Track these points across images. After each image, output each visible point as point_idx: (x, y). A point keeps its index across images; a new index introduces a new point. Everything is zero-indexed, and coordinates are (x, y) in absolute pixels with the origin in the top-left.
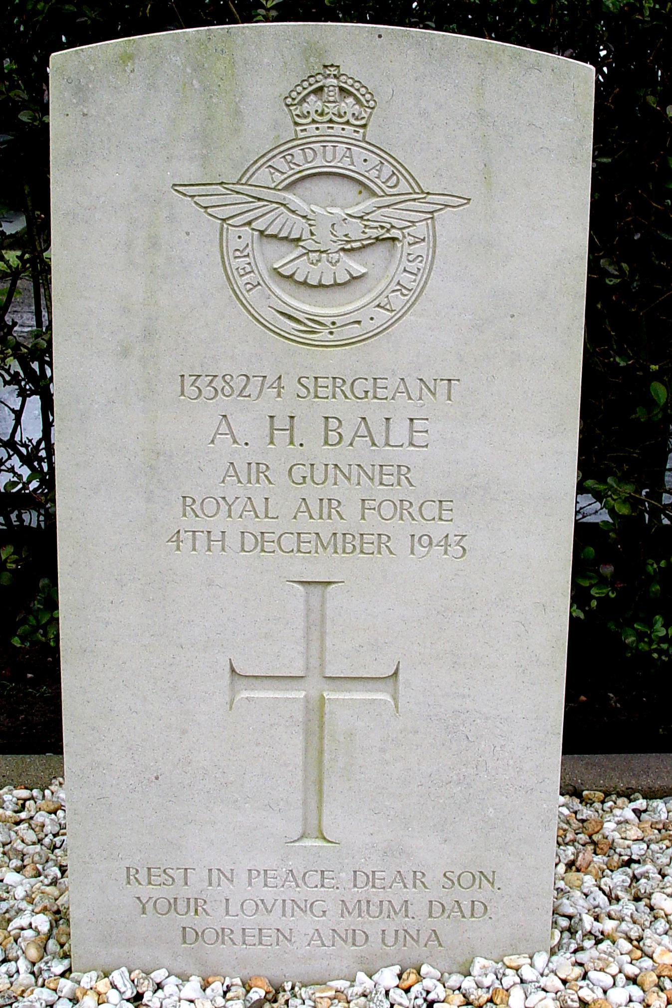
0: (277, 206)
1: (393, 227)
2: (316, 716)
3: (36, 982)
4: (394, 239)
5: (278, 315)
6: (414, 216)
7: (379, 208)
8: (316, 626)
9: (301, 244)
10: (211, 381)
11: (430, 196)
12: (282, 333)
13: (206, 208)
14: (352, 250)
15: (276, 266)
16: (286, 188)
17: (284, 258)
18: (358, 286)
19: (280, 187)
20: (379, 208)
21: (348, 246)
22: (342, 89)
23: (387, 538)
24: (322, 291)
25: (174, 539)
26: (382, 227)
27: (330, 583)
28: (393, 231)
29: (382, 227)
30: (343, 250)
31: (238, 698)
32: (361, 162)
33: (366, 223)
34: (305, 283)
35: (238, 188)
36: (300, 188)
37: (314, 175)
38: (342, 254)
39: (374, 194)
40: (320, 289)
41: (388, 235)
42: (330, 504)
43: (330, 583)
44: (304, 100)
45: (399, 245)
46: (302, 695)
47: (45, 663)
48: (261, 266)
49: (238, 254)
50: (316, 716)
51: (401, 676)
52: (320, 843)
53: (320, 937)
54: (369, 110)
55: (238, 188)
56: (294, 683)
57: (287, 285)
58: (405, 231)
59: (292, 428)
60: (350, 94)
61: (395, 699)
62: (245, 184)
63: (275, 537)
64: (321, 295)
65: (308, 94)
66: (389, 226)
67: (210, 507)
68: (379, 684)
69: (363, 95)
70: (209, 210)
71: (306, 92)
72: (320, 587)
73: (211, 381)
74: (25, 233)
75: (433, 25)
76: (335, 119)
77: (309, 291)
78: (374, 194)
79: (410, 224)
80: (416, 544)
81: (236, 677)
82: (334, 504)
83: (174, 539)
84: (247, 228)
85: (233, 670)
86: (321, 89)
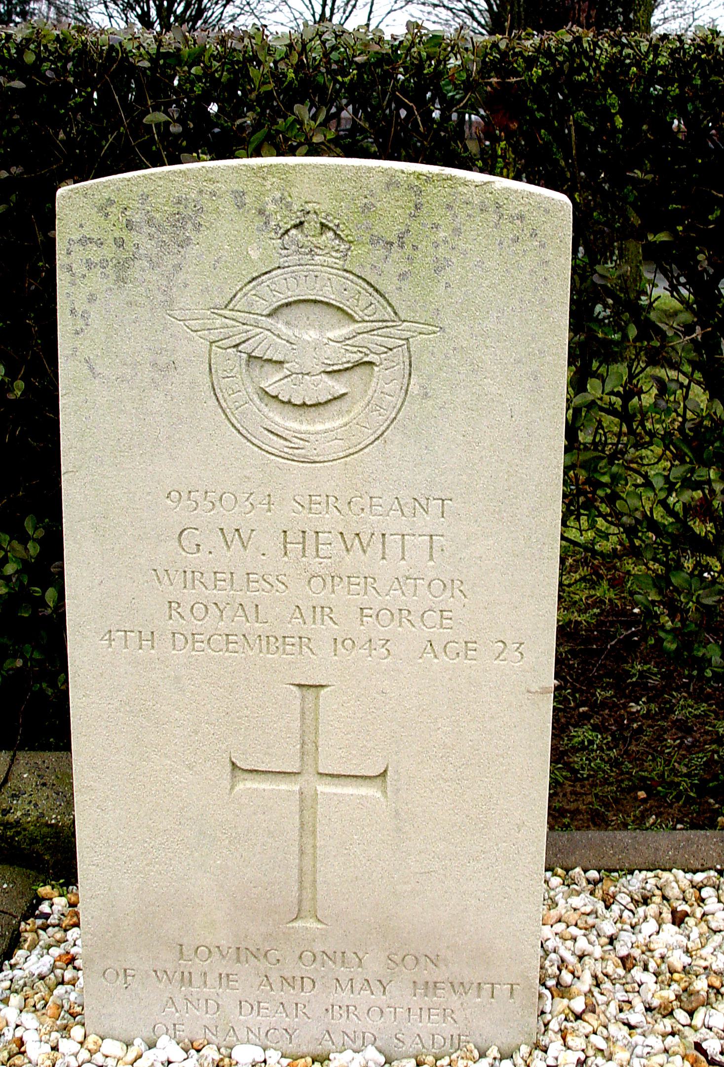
0: (262, 330)
1: (371, 352)
2: (306, 803)
3: (605, 945)
4: (370, 363)
5: (266, 432)
6: (391, 343)
7: (359, 334)
9: (286, 365)
10: (518, 648)
11: (405, 323)
16: (269, 315)
17: (272, 380)
18: (335, 407)
19: (264, 313)
20: (359, 334)
22: (322, 224)
23: (274, 640)
25: (106, 638)
28: (372, 355)
31: (237, 789)
33: (348, 348)
35: (226, 313)
41: (366, 359)
42: (322, 611)
43: (322, 686)
45: (376, 369)
46: (296, 788)
50: (306, 803)
53: (235, 1033)
55: (226, 313)
56: (288, 778)
57: (275, 404)
59: (304, 542)
60: (330, 229)
61: (385, 792)
62: (233, 310)
66: (368, 352)
67: (199, 610)
73: (518, 648)
75: (374, 149)
77: (298, 412)
79: (386, 350)
80: (339, 646)
81: (239, 773)
82: (327, 610)
83: (106, 638)
84: (235, 350)
86: (301, 223)
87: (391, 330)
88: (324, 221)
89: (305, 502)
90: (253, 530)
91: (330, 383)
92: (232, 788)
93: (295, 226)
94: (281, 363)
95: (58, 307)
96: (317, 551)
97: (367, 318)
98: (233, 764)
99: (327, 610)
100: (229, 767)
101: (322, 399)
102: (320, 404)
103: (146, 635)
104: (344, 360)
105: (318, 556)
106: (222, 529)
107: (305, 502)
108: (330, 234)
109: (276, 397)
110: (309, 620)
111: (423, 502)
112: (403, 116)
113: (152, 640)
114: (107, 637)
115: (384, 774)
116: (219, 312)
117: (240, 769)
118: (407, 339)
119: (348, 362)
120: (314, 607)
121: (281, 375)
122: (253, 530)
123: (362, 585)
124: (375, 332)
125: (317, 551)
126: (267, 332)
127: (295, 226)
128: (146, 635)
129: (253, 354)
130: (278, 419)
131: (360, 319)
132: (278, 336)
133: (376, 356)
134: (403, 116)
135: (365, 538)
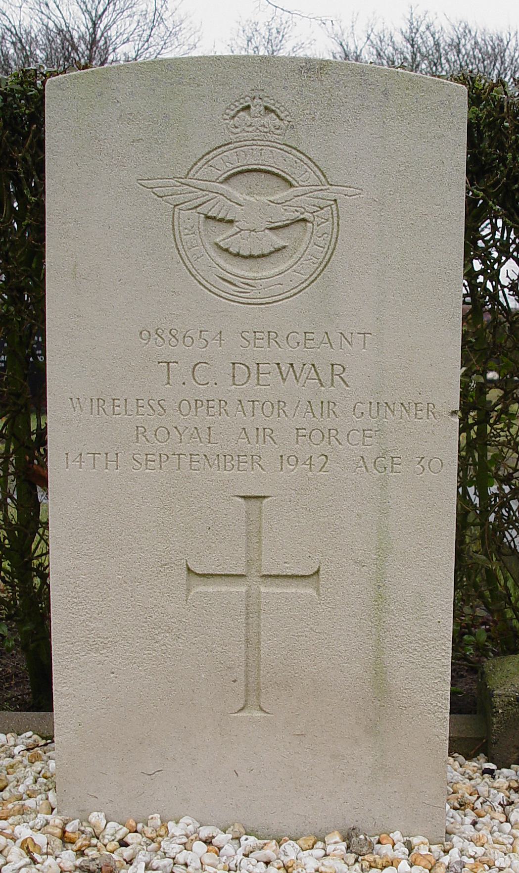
2: (252, 609)
4: (304, 220)
5: (221, 281)
6: (322, 203)
8: (254, 534)
12: (223, 294)
15: (217, 240)
16: (221, 183)
17: (223, 235)
21: (273, 225)
22: (266, 108)
24: (238, 259)
26: (297, 211)
27: (264, 497)
29: (297, 211)
34: (238, 255)
36: (234, 181)
37: (273, 174)
38: (267, 231)
39: (291, 185)
41: (302, 217)
43: (264, 497)
44: (233, 117)
45: (310, 225)
46: (243, 589)
47: (32, 613)
50: (252, 609)
52: (261, 714)
57: (226, 254)
60: (273, 111)
65: (238, 112)
69: (274, 105)
71: (238, 109)
74: (516, 314)
76: (247, 129)
78: (291, 185)
86: (248, 107)
87: (325, 193)
89: (249, 335)
91: (274, 238)
92: (189, 590)
93: (243, 109)
94: (231, 222)
96: (258, 380)
98: (189, 569)
101: (256, 253)
102: (263, 256)
104: (284, 218)
105: (258, 384)
107: (249, 335)
109: (227, 250)
110: (318, 415)
111: (348, 336)
112: (478, 281)
114: (78, 459)
115: (318, 572)
116: (183, 181)
118: (335, 200)
121: (230, 233)
123: (250, 462)
125: (258, 380)
126: (222, 197)
127: (243, 109)
129: (209, 214)
130: (228, 267)
134: (478, 281)
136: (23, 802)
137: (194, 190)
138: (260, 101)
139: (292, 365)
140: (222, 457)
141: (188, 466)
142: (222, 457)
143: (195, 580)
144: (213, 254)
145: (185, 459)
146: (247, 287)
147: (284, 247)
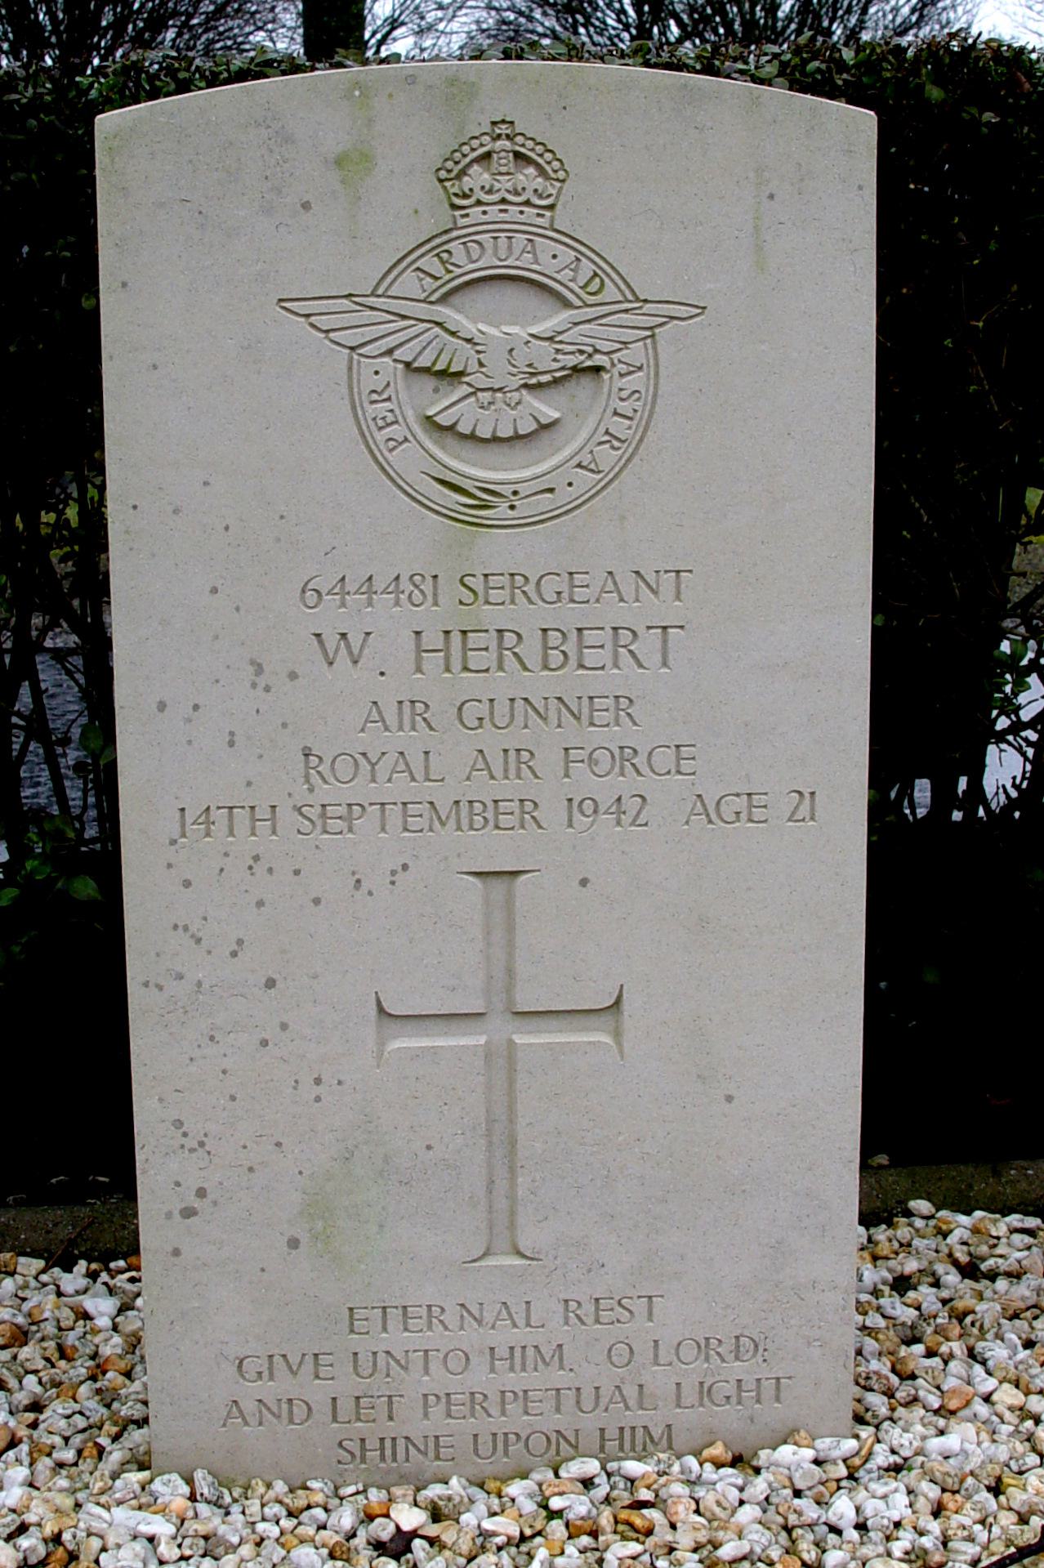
0: (429, 325)
1: (597, 351)
2: (504, 1062)
4: (597, 370)
7: (576, 324)
9: (466, 379)
13: (327, 331)
14: (540, 385)
16: (443, 299)
17: (446, 404)
19: (433, 299)
20: (576, 324)
21: (533, 381)
22: (518, 155)
24: (519, 444)
28: (597, 356)
29: (581, 352)
30: (525, 386)
32: (551, 260)
36: (456, 299)
38: (524, 392)
40: (494, 447)
41: (589, 363)
45: (606, 376)
48: (410, 413)
49: (375, 397)
50: (504, 1062)
51: (626, 1005)
54: (558, 185)
55: (372, 301)
58: (613, 356)
60: (529, 161)
61: (617, 1034)
63: (583, 754)
64: (494, 453)
66: (590, 349)
68: (593, 1020)
70: (332, 335)
71: (468, 160)
72: (506, 878)
79: (619, 346)
84: (386, 359)
85: (381, 1010)
86: (487, 156)
88: (522, 150)
90: (368, 634)
91: (536, 404)
95: (98, 172)
97: (591, 299)
99: (525, 755)
100: (373, 1011)
103: (263, 812)
104: (556, 365)
106: (318, 635)
107: (476, 583)
108: (531, 171)
111: (651, 578)
113: (273, 819)
117: (390, 1015)
119: (563, 368)
120: (506, 751)
122: (368, 634)
124: (603, 321)
126: (437, 330)
128: (263, 812)
131: (580, 304)
132: (453, 334)
133: (605, 358)
135: (355, 640)
136: (433, 1530)
137: (392, 318)
138: (508, 143)
139: (344, 635)
140: (464, 806)
141: (400, 823)
142: (464, 806)
143: (386, 1020)
144: (421, 435)
145: (394, 812)
146: (485, 496)
147: (555, 422)
